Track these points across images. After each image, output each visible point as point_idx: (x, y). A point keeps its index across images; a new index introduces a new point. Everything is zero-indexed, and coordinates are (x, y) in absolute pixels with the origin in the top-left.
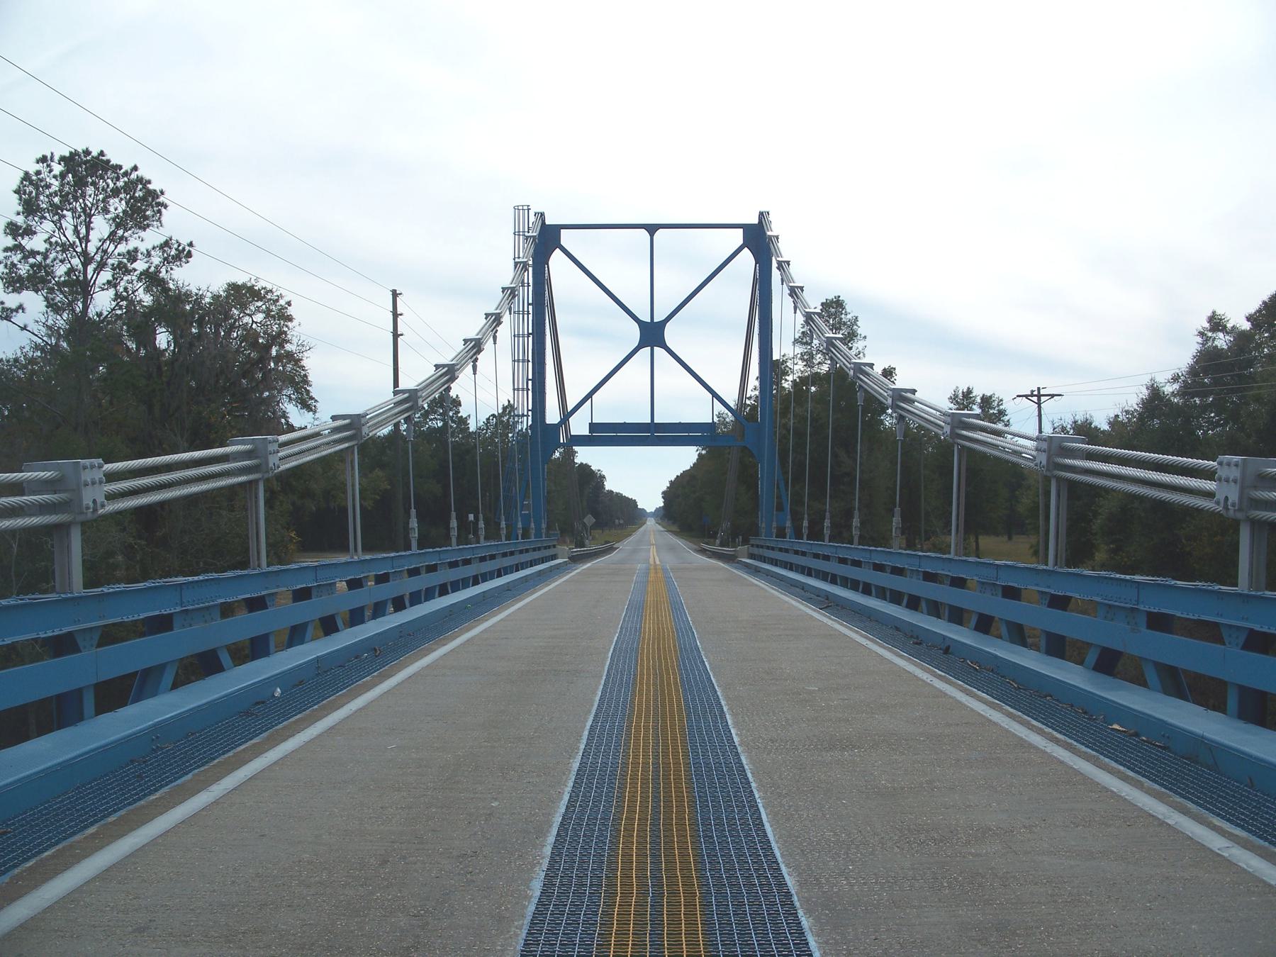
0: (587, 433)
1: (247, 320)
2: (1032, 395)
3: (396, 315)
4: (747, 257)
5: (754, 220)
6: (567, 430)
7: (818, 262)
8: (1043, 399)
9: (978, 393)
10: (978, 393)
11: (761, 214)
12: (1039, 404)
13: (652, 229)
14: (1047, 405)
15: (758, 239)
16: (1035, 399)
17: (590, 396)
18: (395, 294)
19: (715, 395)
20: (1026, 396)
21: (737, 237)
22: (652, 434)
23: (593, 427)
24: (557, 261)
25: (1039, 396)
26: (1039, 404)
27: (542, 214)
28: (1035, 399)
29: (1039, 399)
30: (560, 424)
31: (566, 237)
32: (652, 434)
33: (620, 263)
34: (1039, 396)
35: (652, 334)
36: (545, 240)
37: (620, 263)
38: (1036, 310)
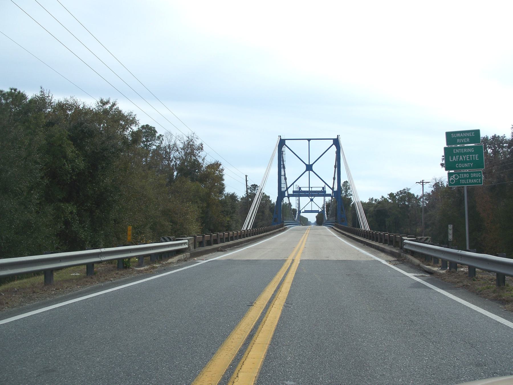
0: (292, 193)
3: (246, 181)
4: (334, 148)
5: (336, 138)
6: (288, 192)
7: (339, 137)
9: (374, 198)
10: (374, 198)
12: (423, 185)
13: (309, 140)
15: (336, 142)
17: (293, 184)
18: (246, 176)
22: (311, 194)
23: (294, 192)
24: (285, 149)
26: (423, 185)
30: (285, 191)
31: (287, 142)
32: (311, 194)
34: (423, 183)
35: (309, 168)
36: (282, 143)
37: (300, 148)
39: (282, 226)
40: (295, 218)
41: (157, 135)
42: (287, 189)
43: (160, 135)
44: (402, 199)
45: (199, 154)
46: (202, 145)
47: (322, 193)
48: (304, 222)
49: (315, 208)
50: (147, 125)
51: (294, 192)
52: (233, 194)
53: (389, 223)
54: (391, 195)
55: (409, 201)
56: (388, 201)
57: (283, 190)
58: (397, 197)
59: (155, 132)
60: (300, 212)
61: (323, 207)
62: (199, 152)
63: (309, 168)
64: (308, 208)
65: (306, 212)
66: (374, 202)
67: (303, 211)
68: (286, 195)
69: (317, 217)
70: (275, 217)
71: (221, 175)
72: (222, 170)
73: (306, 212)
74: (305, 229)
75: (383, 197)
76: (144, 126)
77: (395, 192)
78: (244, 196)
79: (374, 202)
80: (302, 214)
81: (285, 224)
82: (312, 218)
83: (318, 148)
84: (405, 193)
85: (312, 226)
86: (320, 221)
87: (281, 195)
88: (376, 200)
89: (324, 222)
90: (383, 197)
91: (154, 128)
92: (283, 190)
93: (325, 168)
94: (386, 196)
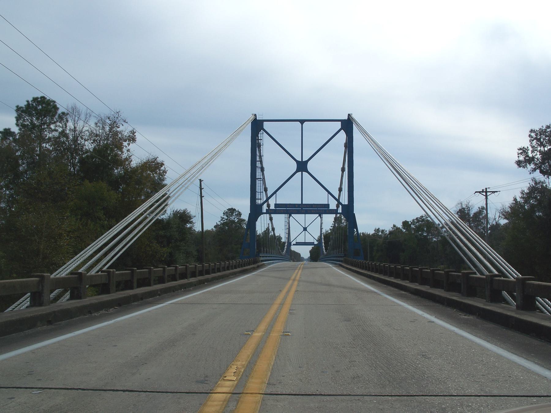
1: (165, 256)
2: (483, 192)
3: (201, 189)
4: (343, 135)
5: (346, 118)
8: (488, 194)
9: (381, 229)
11: (349, 115)
12: (486, 196)
13: (302, 122)
14: (491, 197)
15: (348, 125)
16: (484, 194)
17: (275, 192)
18: (201, 181)
19: (329, 193)
20: (480, 192)
21: (339, 125)
23: (276, 205)
24: (264, 139)
25: (486, 192)
26: (486, 196)
27: (255, 115)
28: (484, 194)
29: (486, 194)
31: (266, 125)
33: (288, 135)
34: (486, 192)
35: (305, 229)
36: (257, 126)
38: (473, 167)
39: (255, 262)
40: (273, 248)
41: (60, 112)
42: (338, 200)
43: (63, 113)
44: (419, 229)
45: (129, 148)
46: (133, 132)
47: (321, 210)
48: (296, 257)
49: (309, 239)
50: (43, 98)
51: (276, 205)
52: (184, 211)
53: (414, 260)
54: (405, 224)
55: (428, 232)
56: (401, 230)
57: (259, 202)
58: (413, 226)
59: (56, 108)
60: (290, 244)
61: (319, 240)
62: (129, 144)
63: (305, 229)
64: (301, 239)
65: (298, 244)
66: (380, 233)
67: (294, 242)
68: (264, 210)
69: (311, 252)
70: (239, 247)
71: (160, 179)
72: (165, 172)
73: (298, 244)
74: (294, 268)
75: (394, 226)
76: (37, 98)
77: (410, 219)
78: (219, 223)
79: (380, 233)
80: (293, 248)
81: (262, 259)
82: (305, 252)
83: (316, 135)
84: (423, 220)
85: (305, 262)
86: (315, 256)
87: (256, 211)
88: (383, 231)
89: (321, 257)
90: (394, 226)
91: (54, 102)
92: (259, 202)
93: (328, 166)
94: (400, 225)
